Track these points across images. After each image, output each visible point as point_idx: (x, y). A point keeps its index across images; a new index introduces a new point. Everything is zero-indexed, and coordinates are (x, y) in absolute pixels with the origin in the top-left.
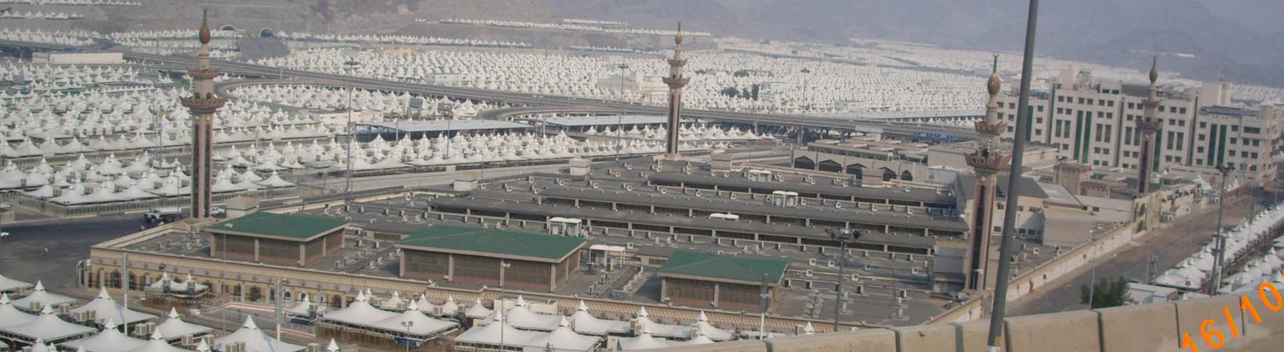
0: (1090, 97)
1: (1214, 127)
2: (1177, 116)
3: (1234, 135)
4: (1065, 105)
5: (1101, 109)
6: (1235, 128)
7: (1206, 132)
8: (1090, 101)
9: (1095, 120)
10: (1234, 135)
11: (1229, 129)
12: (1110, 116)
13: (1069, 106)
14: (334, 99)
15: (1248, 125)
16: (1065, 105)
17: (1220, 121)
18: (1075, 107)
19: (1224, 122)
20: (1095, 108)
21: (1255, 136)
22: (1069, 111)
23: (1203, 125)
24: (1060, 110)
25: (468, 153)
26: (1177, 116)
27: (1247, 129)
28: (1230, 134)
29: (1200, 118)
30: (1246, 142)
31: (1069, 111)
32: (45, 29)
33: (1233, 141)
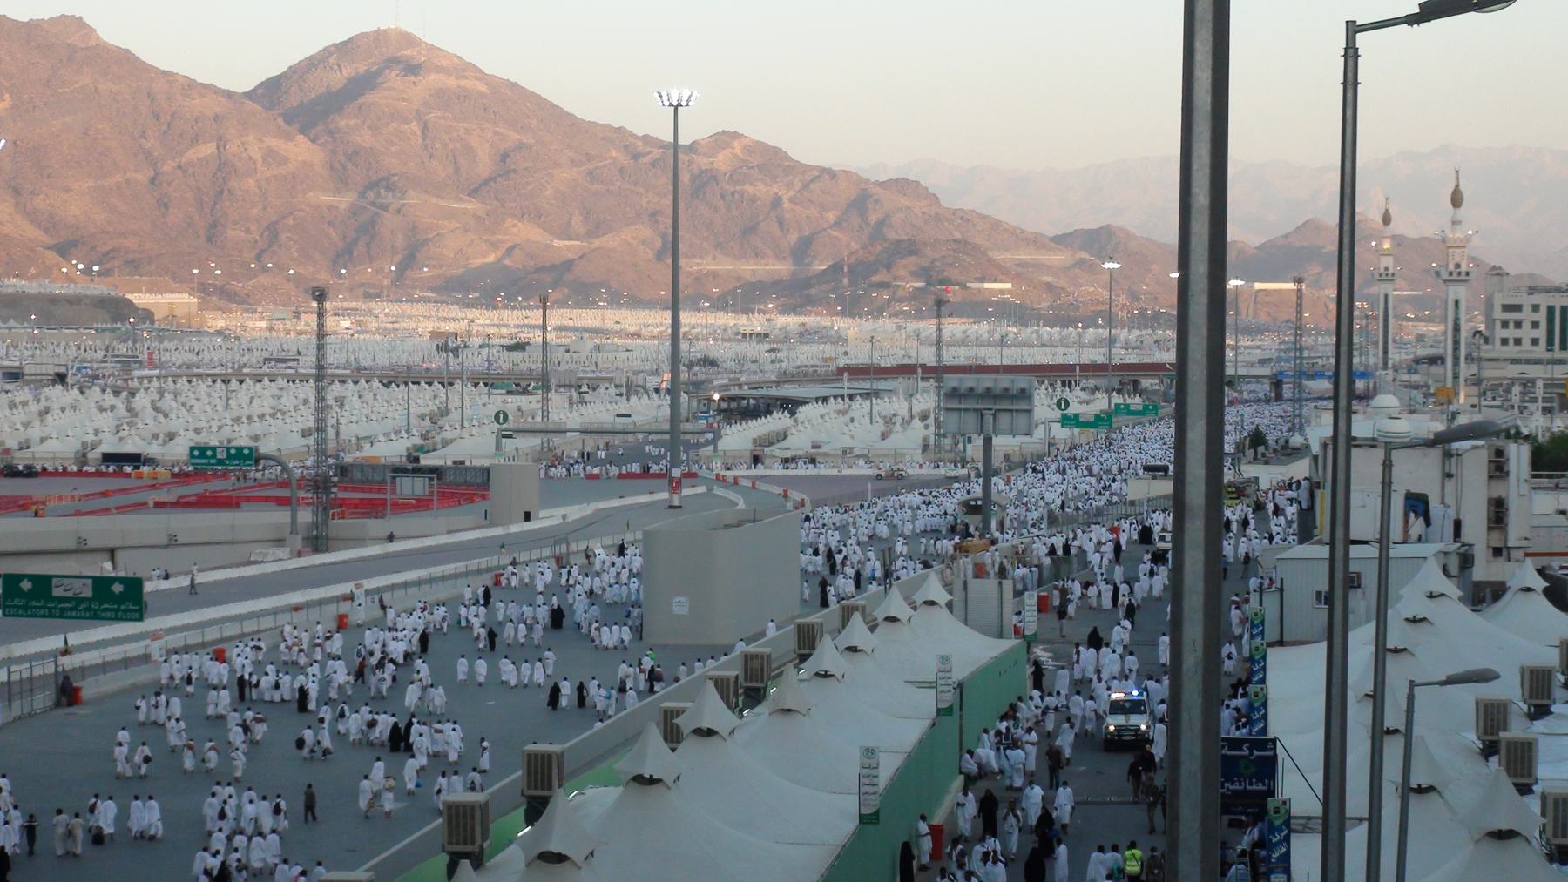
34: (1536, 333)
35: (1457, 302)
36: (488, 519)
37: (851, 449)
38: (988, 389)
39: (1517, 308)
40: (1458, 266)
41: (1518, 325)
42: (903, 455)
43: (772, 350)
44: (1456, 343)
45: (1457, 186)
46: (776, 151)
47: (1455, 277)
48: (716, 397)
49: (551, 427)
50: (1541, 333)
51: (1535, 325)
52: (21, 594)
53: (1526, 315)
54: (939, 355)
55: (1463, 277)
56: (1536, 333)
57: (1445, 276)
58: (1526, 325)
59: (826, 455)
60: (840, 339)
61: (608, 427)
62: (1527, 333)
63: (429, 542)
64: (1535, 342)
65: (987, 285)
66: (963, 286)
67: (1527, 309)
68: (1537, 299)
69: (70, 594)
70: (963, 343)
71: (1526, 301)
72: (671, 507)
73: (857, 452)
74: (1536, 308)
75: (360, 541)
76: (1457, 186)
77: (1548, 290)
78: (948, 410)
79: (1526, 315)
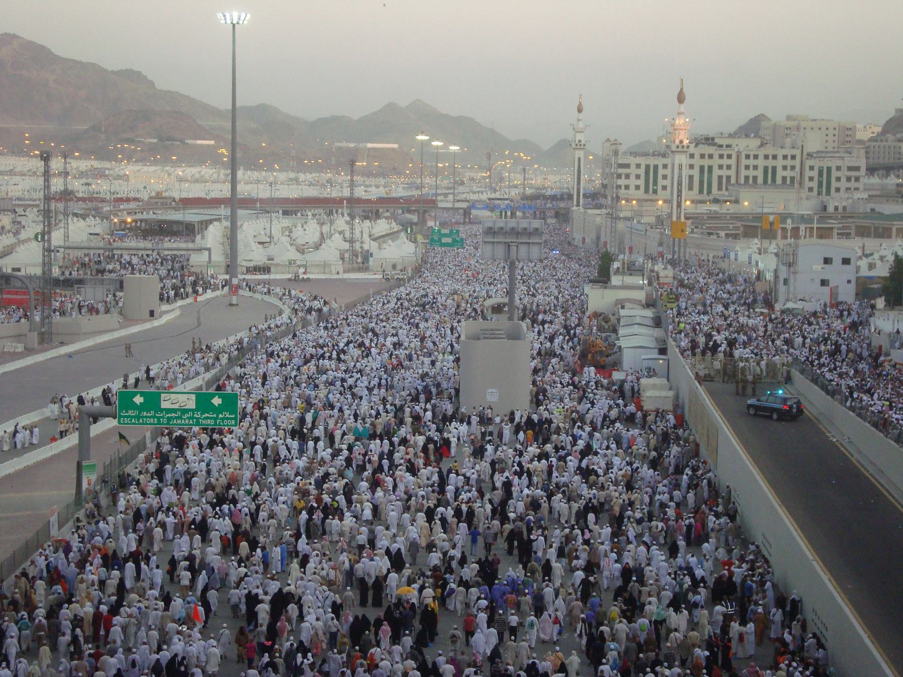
0: (774, 153)
1: (648, 167)
2: (789, 162)
3: (839, 174)
4: (752, 162)
5: (721, 162)
6: (838, 168)
7: (815, 174)
8: (711, 156)
9: (716, 172)
10: (839, 174)
11: (660, 167)
12: (747, 167)
13: (755, 162)
14: (464, 196)
15: (850, 164)
16: (752, 162)
17: (652, 161)
18: (761, 162)
19: (830, 164)
20: (716, 161)
21: (856, 174)
22: (755, 168)
23: (812, 168)
24: (729, 167)
25: (213, 195)
26: (789, 162)
27: (850, 169)
28: (835, 174)
29: (809, 163)
30: (849, 179)
31: (755, 168)
32: (207, 177)
33: (838, 179)
34: (638, 182)
35: (579, 159)
36: (128, 319)
37: (294, 261)
38: (513, 229)
39: (627, 166)
40: (681, 142)
41: (627, 176)
42: (330, 265)
43: (88, 184)
44: (579, 189)
45: (682, 89)
46: (42, 48)
47: (680, 149)
48: (129, 220)
49: (71, 245)
50: (641, 182)
51: (638, 177)
52: (134, 406)
53: (633, 171)
54: (352, 193)
55: (685, 149)
56: (638, 182)
57: (574, 146)
58: (632, 177)
59: (277, 265)
60: (126, 178)
61: (85, 245)
62: (633, 182)
63: (106, 337)
64: (637, 187)
65: (199, 142)
66: (182, 142)
67: (633, 167)
68: (639, 160)
69: (176, 406)
70: (258, 182)
71: (633, 161)
72: (231, 305)
73: (298, 263)
74: (638, 166)
75: (75, 336)
76: (682, 89)
77: (646, 155)
78: (485, 242)
79: (633, 171)
